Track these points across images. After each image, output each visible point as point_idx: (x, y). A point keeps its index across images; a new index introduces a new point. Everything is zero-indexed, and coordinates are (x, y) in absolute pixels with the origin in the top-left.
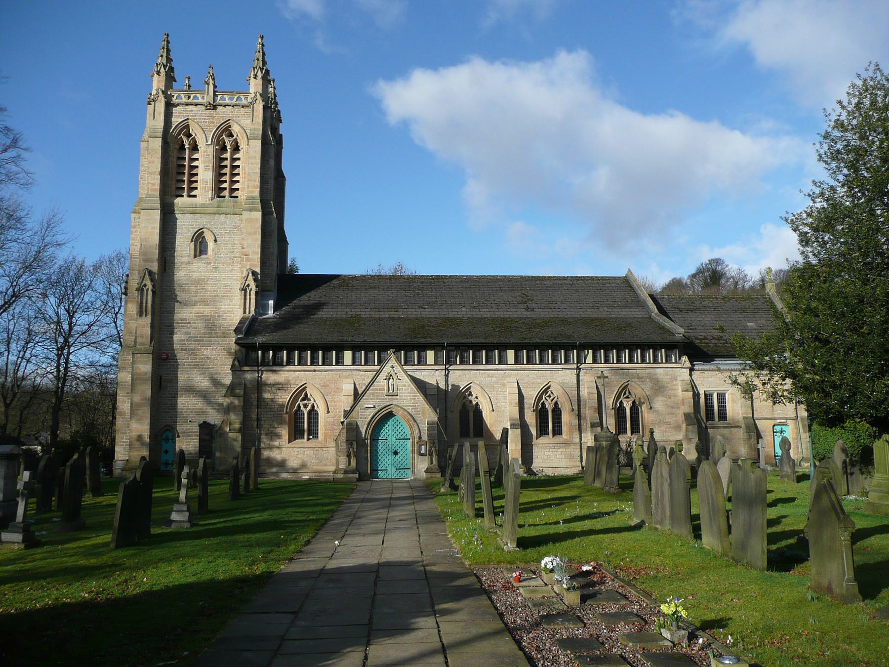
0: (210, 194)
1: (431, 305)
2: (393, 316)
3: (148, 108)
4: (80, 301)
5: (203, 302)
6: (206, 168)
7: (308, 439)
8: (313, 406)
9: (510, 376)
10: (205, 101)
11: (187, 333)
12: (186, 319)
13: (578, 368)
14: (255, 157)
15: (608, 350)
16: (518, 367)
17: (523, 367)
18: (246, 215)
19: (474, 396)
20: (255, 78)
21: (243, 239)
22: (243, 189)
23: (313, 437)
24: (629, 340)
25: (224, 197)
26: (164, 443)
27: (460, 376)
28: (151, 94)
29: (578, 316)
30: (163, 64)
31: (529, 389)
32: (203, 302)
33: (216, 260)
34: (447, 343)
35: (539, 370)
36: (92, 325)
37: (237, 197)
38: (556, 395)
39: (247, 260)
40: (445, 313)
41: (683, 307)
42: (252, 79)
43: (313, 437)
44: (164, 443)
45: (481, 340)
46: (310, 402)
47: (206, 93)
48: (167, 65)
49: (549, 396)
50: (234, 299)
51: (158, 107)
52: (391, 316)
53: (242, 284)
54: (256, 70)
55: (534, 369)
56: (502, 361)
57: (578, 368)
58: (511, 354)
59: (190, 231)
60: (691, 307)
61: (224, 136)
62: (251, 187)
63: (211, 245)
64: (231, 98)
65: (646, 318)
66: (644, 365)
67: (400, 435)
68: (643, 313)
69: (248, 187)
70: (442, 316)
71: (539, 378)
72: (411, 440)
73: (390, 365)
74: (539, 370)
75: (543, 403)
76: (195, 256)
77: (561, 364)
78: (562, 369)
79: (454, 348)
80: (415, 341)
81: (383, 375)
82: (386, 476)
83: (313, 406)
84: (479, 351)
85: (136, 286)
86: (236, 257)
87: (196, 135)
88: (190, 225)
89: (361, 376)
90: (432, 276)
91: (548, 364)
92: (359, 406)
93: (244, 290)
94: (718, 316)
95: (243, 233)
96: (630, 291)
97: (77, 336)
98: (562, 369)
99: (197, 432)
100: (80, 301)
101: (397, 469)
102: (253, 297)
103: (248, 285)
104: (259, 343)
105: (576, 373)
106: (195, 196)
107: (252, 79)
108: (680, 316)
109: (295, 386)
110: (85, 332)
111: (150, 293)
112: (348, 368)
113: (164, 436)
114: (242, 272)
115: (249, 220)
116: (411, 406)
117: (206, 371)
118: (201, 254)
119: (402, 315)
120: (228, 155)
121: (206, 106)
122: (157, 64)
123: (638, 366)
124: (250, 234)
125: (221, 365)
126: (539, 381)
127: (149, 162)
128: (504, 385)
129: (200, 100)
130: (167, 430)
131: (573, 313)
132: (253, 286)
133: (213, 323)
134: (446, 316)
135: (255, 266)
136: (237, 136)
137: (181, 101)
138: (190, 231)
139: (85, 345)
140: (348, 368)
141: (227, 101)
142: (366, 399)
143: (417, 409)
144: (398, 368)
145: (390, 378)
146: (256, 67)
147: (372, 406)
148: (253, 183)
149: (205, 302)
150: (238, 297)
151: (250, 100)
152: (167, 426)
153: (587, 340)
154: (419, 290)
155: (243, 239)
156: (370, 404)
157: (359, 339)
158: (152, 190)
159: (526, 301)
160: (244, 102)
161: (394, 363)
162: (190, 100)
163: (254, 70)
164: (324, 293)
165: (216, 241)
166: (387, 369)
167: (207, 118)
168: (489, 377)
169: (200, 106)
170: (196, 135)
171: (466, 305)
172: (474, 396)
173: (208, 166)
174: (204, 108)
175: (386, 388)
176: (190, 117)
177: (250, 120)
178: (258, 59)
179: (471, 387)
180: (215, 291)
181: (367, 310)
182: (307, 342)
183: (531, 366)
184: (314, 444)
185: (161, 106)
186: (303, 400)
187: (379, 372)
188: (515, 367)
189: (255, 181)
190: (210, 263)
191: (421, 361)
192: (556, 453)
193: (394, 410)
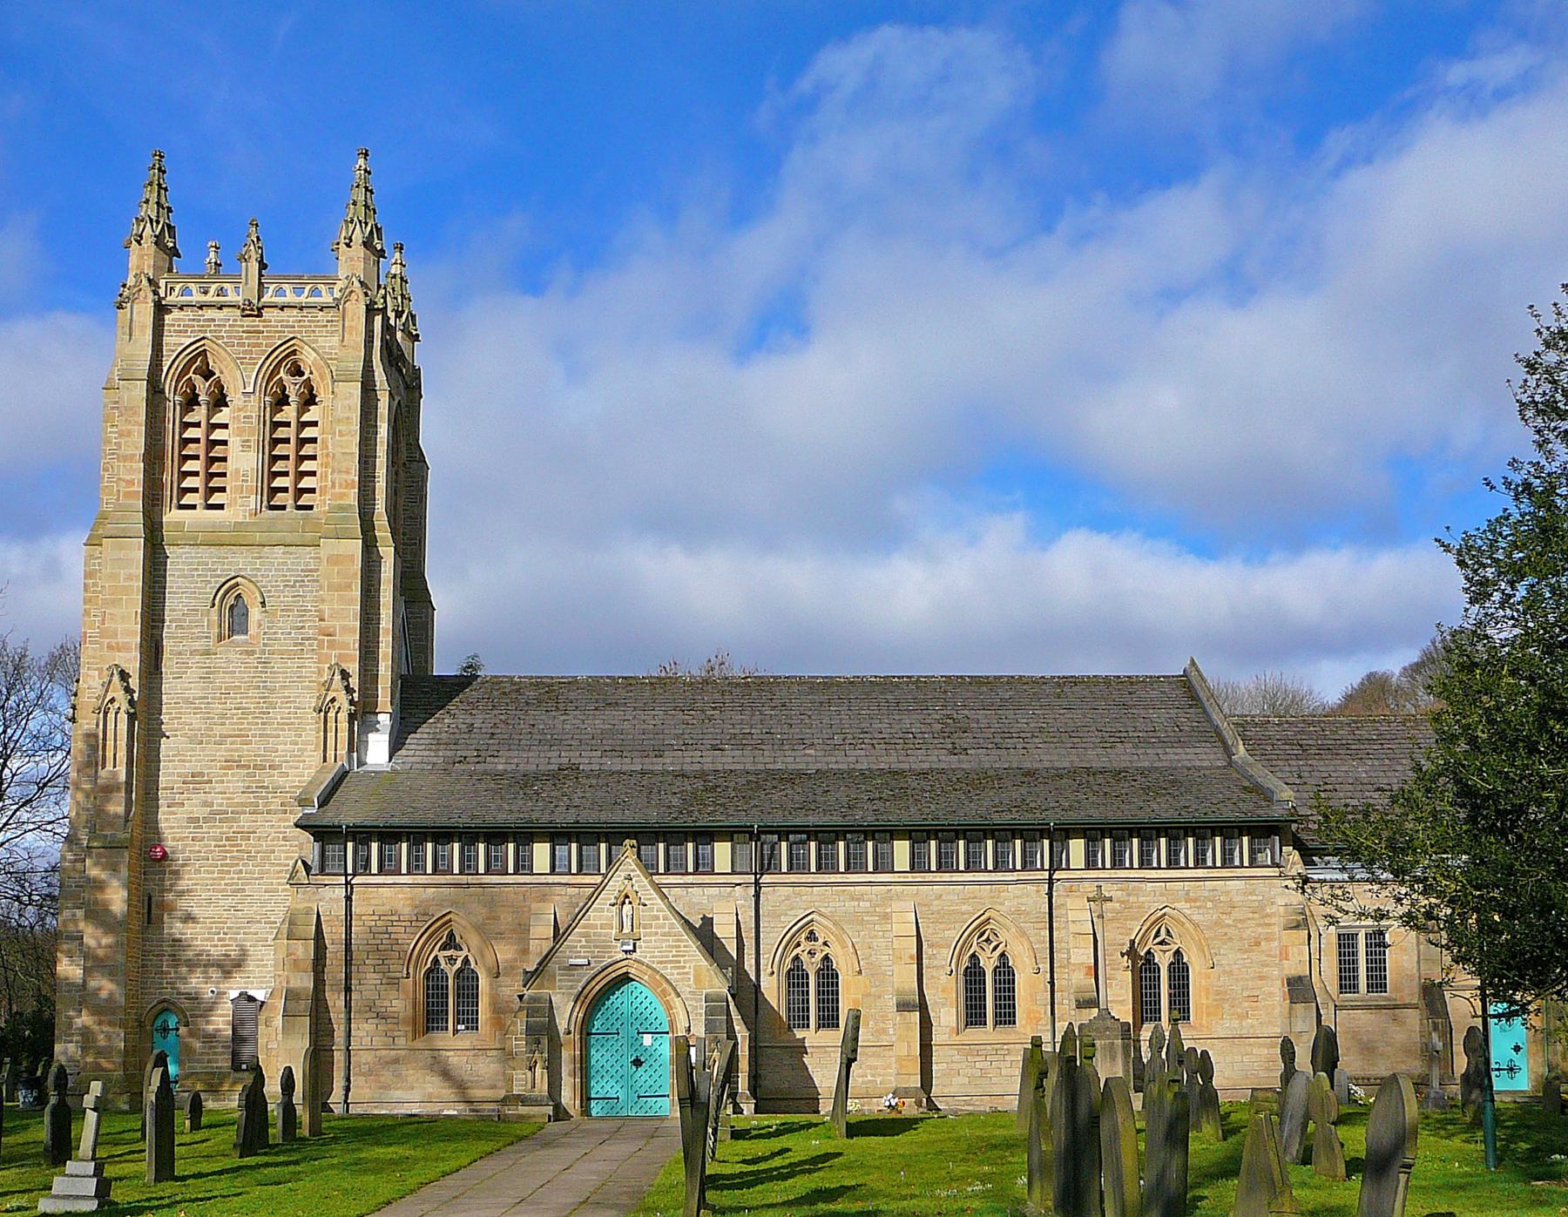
0: (253, 501)
1: (739, 741)
2: (651, 767)
3: (119, 315)
4: (19, 732)
5: (238, 736)
6: (245, 445)
7: (456, 1031)
8: (466, 961)
9: (899, 897)
10: (239, 299)
11: (205, 804)
12: (202, 774)
13: (1051, 882)
14: (348, 418)
15: (1204, 838)
16: (919, 877)
17: (929, 877)
18: (329, 547)
19: (821, 941)
20: (348, 245)
21: (323, 601)
22: (324, 491)
23: (467, 1028)
24: (1230, 814)
25: (283, 508)
26: (157, 1037)
27: (788, 898)
28: (124, 286)
29: (1067, 765)
30: (151, 220)
31: (942, 926)
32: (238, 736)
33: (264, 645)
34: (759, 826)
35: (963, 884)
36: (45, 785)
37: (310, 508)
38: (1001, 939)
39: (332, 645)
40: (767, 760)
41: (1310, 742)
42: (342, 247)
43: (467, 1028)
44: (157, 1037)
45: (836, 820)
46: (459, 953)
47: (243, 280)
48: (366, 224)
49: (987, 940)
50: (305, 730)
51: (139, 313)
52: (645, 768)
53: (318, 698)
54: (351, 227)
55: (1127, 879)
56: (884, 864)
57: (1051, 882)
58: (902, 849)
59: (210, 582)
60: (1330, 742)
61: (282, 374)
62: (341, 485)
63: (255, 613)
64: (298, 291)
65: (1219, 767)
66: (1200, 873)
67: (646, 1025)
68: (1212, 757)
69: (333, 486)
70: (760, 767)
71: (965, 901)
72: (671, 1035)
73: (623, 874)
74: (963, 884)
75: (973, 955)
76: (220, 638)
77: (1014, 870)
78: (1017, 882)
79: (804, 836)
80: (686, 821)
81: (609, 894)
82: (615, 1111)
83: (466, 961)
84: (833, 843)
85: (95, 703)
86: (308, 639)
87: (222, 372)
88: (210, 570)
89: (571, 896)
90: (988, 677)
91: (986, 870)
92: (555, 963)
93: (322, 710)
94: (1387, 761)
95: (321, 588)
96: (1191, 706)
97: (15, 807)
98: (1017, 882)
99: (228, 1015)
100: (19, 732)
101: (639, 1097)
102: (344, 725)
103: (112, 701)
104: (348, 827)
105: (344, 894)
106: (221, 507)
107: (342, 247)
108: (1301, 763)
109: (426, 918)
110: (30, 801)
111: (123, 717)
112: (543, 879)
113: (159, 1023)
114: (320, 673)
115: (334, 560)
116: (671, 962)
117: (247, 884)
118: (232, 632)
119: (672, 764)
120: (289, 413)
121: (243, 310)
122: (346, 221)
123: (1132, 874)
124: (339, 588)
125: (278, 873)
126: (964, 908)
127: (121, 436)
128: (886, 917)
129: (232, 297)
130: (165, 1010)
131: (1056, 758)
132: (343, 700)
133: (259, 781)
134: (768, 766)
135: (348, 658)
136: (311, 373)
137: (189, 298)
138: (210, 582)
139: (32, 826)
140: (721, 879)
141: (290, 298)
142: (568, 947)
143: (684, 967)
144: (641, 882)
145: (624, 903)
146: (352, 222)
147: (585, 961)
148: (344, 476)
149: (243, 736)
150: (311, 731)
151: (337, 295)
152: (164, 1001)
153: (1072, 817)
154: (714, 709)
155: (323, 601)
156: (579, 957)
157: (564, 817)
158: (128, 495)
159: (952, 732)
160: (326, 298)
161: (633, 870)
162: (208, 298)
163: (347, 227)
164: (502, 717)
165: (263, 604)
166: (616, 883)
167: (245, 335)
168: (853, 899)
169: (230, 309)
170: (222, 372)
171: (816, 741)
172: (821, 941)
173: (248, 441)
174: (238, 312)
175: (615, 922)
176: (208, 335)
177: (336, 339)
178: (355, 203)
179: (450, 920)
180: (264, 713)
181: (594, 753)
182: (454, 822)
183: (947, 877)
184: (468, 1043)
185: (143, 312)
186: (443, 948)
187: (598, 889)
188: (910, 877)
189: (348, 472)
190: (253, 653)
191: (704, 866)
192: (1002, 1065)
193: (632, 971)
